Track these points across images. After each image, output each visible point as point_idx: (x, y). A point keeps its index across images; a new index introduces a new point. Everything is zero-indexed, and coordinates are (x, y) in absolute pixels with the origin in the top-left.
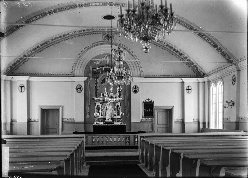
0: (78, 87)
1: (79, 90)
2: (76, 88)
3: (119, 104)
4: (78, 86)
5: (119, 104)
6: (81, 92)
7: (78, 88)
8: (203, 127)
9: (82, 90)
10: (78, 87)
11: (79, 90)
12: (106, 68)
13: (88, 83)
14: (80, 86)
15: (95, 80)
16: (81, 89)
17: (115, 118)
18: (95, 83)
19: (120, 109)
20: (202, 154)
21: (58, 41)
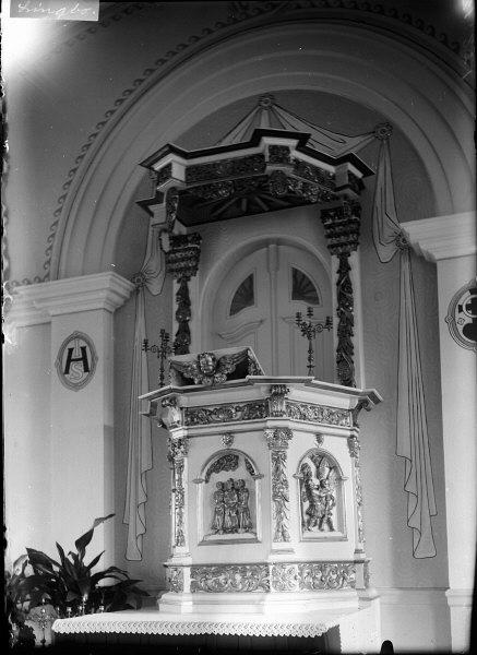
0: (71, 351)
1: (77, 368)
2: (60, 358)
3: (336, 447)
4: (70, 346)
5: (336, 447)
6: (86, 381)
7: (69, 360)
8: (43, 641)
9: (94, 365)
10: (71, 351)
11: (77, 368)
12: (197, 167)
13: (141, 321)
14: (83, 344)
15: (176, 287)
16: (84, 359)
17: (282, 564)
18: (176, 307)
19: (349, 488)
20: (103, 192)
21: (84, 163)
